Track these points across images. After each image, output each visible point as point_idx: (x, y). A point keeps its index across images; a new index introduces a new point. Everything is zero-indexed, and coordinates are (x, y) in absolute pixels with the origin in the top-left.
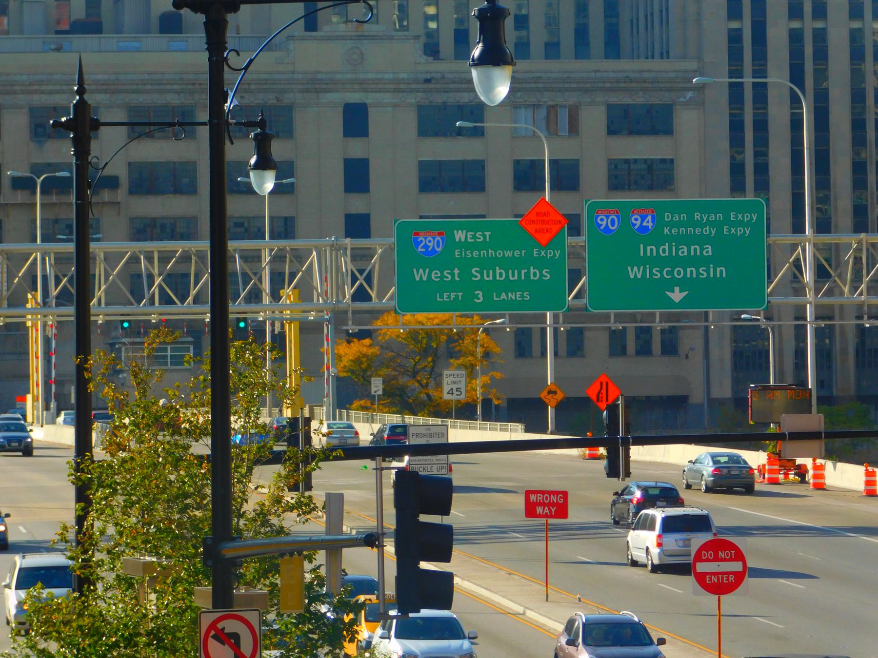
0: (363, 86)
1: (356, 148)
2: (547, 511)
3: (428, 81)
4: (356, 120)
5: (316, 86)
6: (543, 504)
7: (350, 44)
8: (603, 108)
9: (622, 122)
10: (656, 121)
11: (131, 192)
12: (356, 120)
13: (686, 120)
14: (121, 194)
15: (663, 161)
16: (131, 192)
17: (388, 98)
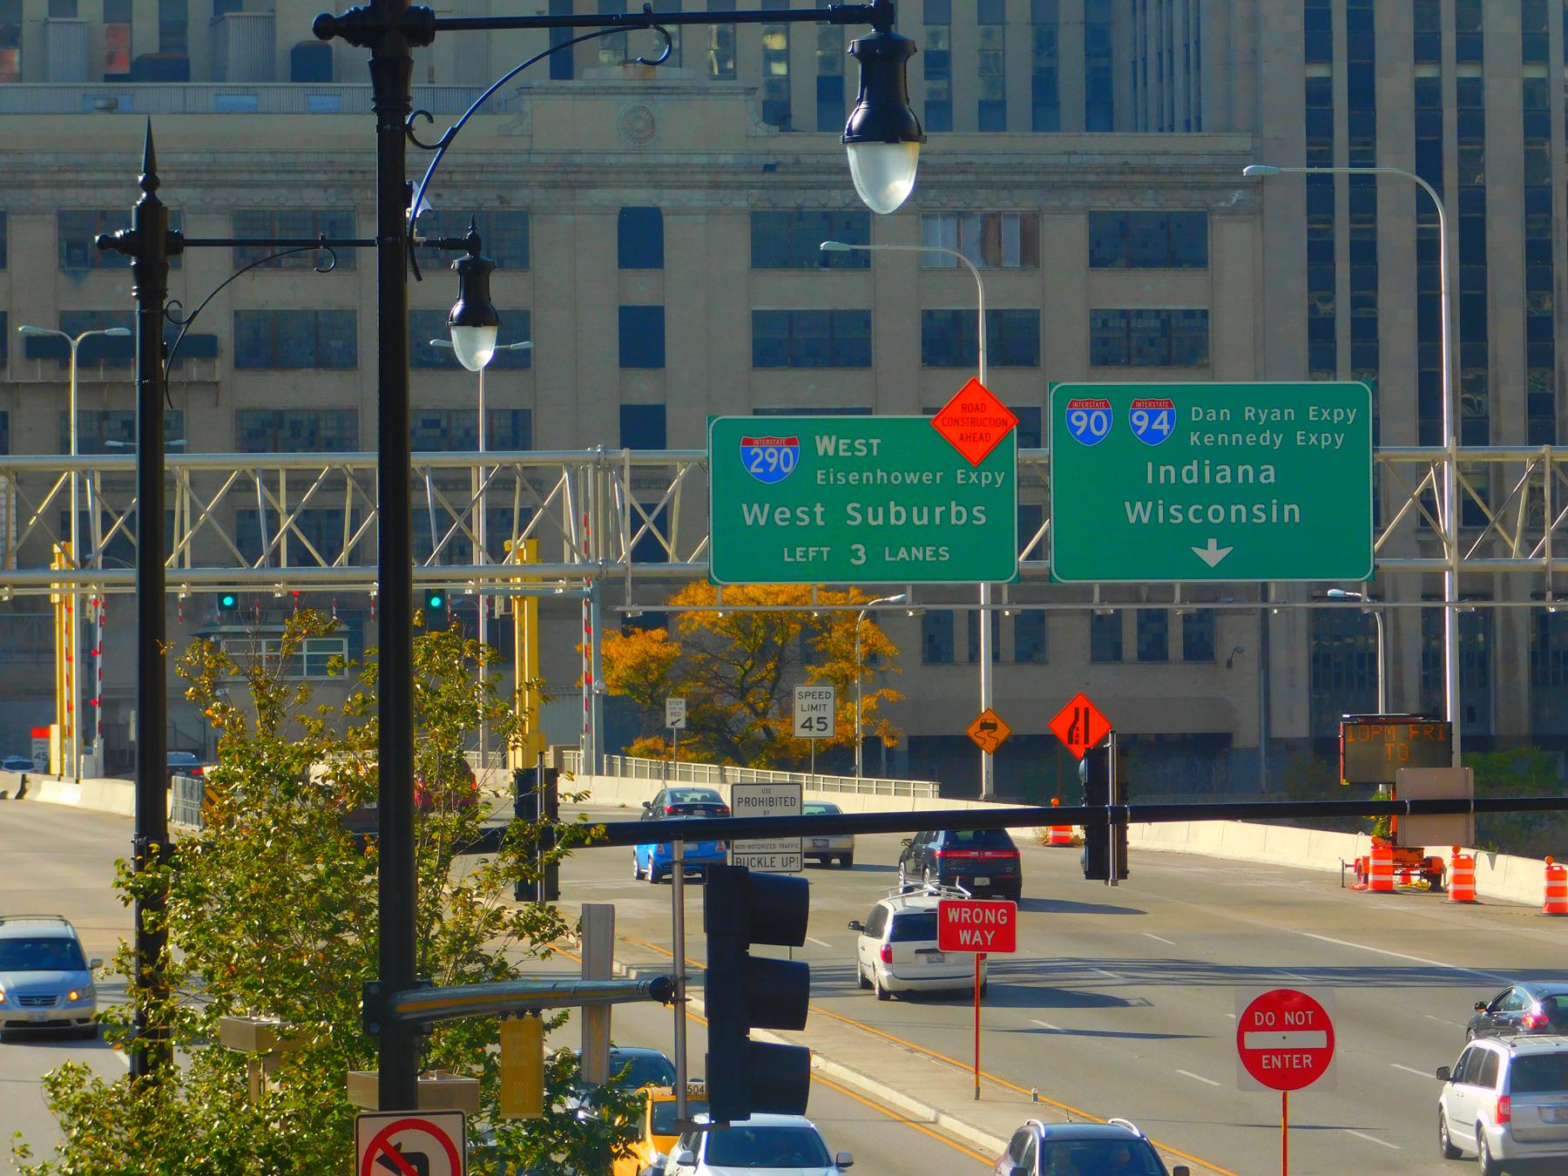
0: (654, 176)
1: (641, 288)
2: (978, 937)
3: (770, 168)
4: (641, 239)
5: (571, 176)
6: (972, 927)
7: (631, 102)
8: (1082, 220)
9: (1116, 243)
10: (1177, 242)
11: (239, 364)
12: (641, 239)
13: (1230, 241)
14: (221, 368)
15: (1189, 314)
16: (239, 364)
17: (697, 198)
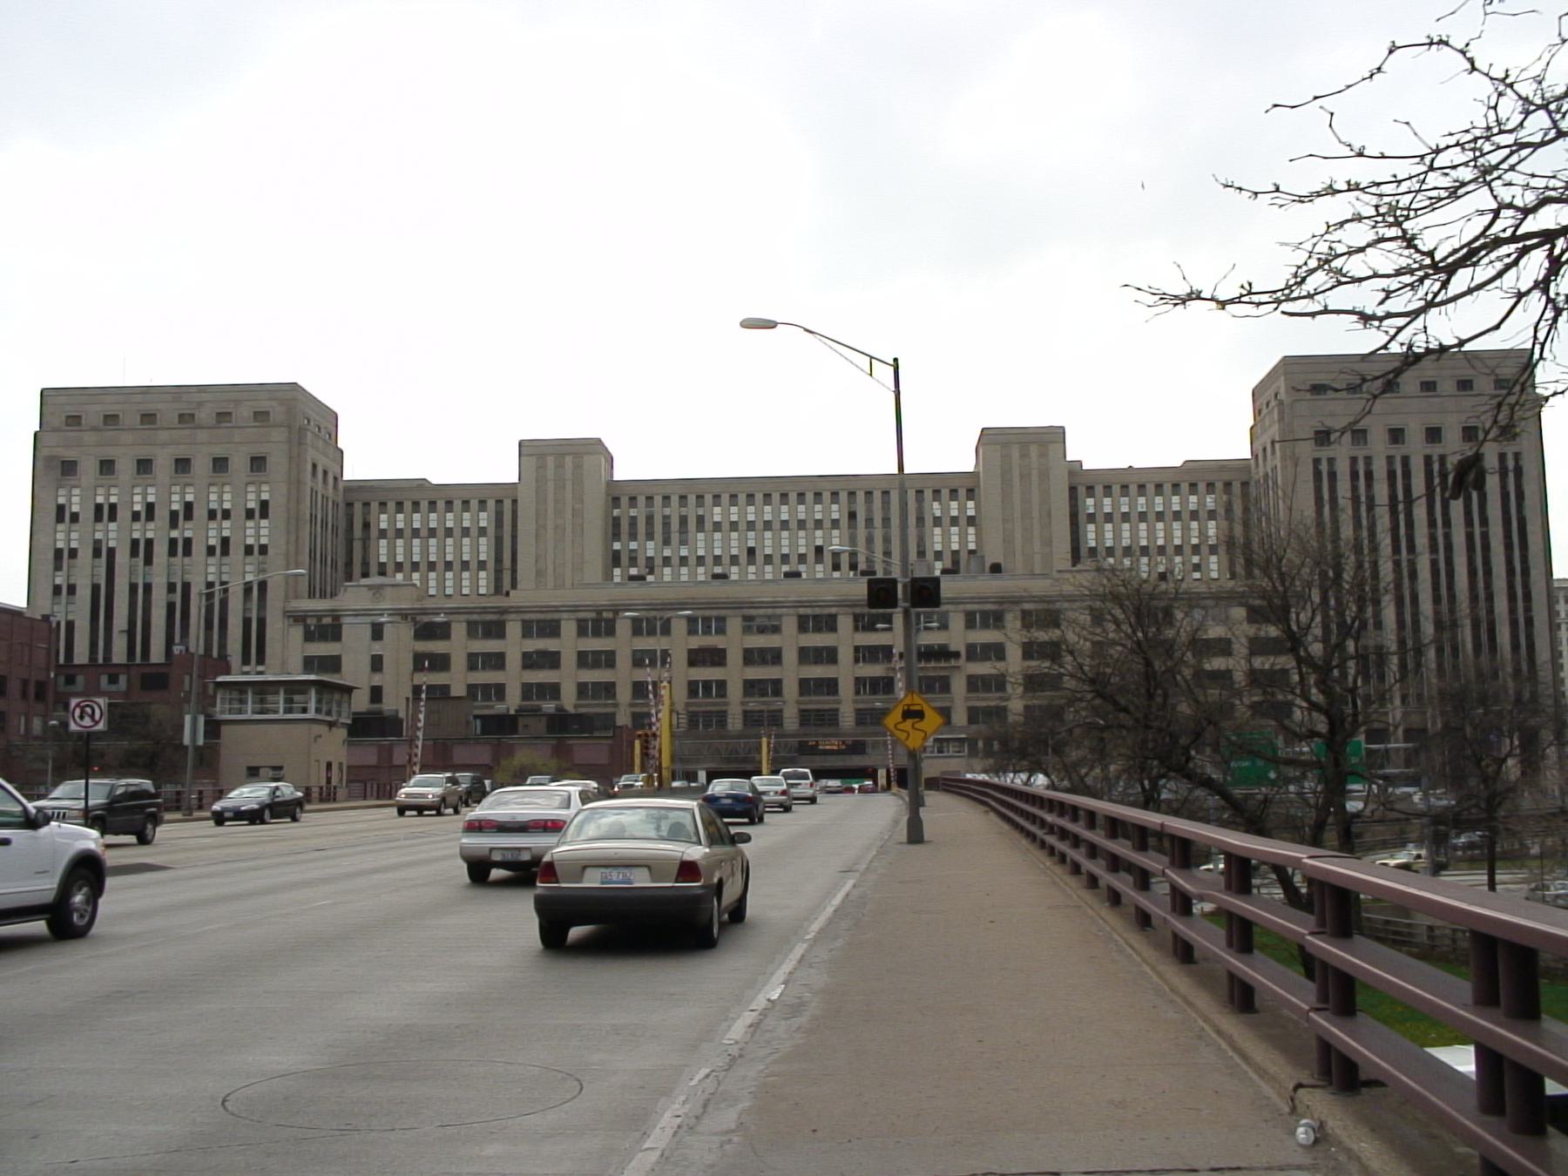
1: (377, 648)
4: (377, 633)
12: (377, 633)
14: (962, 661)
